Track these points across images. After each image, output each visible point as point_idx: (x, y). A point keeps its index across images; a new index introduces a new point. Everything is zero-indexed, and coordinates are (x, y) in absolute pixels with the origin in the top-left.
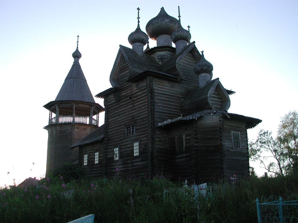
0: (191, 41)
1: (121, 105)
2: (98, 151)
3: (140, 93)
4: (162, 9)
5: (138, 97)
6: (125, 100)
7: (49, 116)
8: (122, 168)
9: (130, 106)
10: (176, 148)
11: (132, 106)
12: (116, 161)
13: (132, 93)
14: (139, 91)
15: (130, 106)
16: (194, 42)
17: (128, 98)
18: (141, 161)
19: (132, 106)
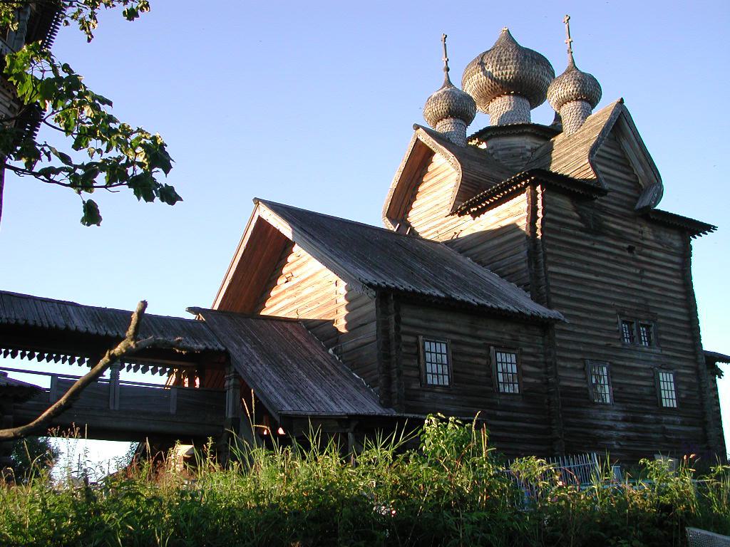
0: (157, 199)
1: (596, 246)
2: (515, 349)
3: (662, 255)
4: (182, 200)
5: (652, 261)
6: (612, 242)
7: (214, 298)
8: (628, 429)
9: (633, 270)
10: (438, 297)
11: (638, 271)
12: (601, 406)
13: (641, 241)
14: (660, 249)
15: (633, 270)
16: (139, 199)
17: (626, 245)
18: (683, 424)
19: (638, 271)
